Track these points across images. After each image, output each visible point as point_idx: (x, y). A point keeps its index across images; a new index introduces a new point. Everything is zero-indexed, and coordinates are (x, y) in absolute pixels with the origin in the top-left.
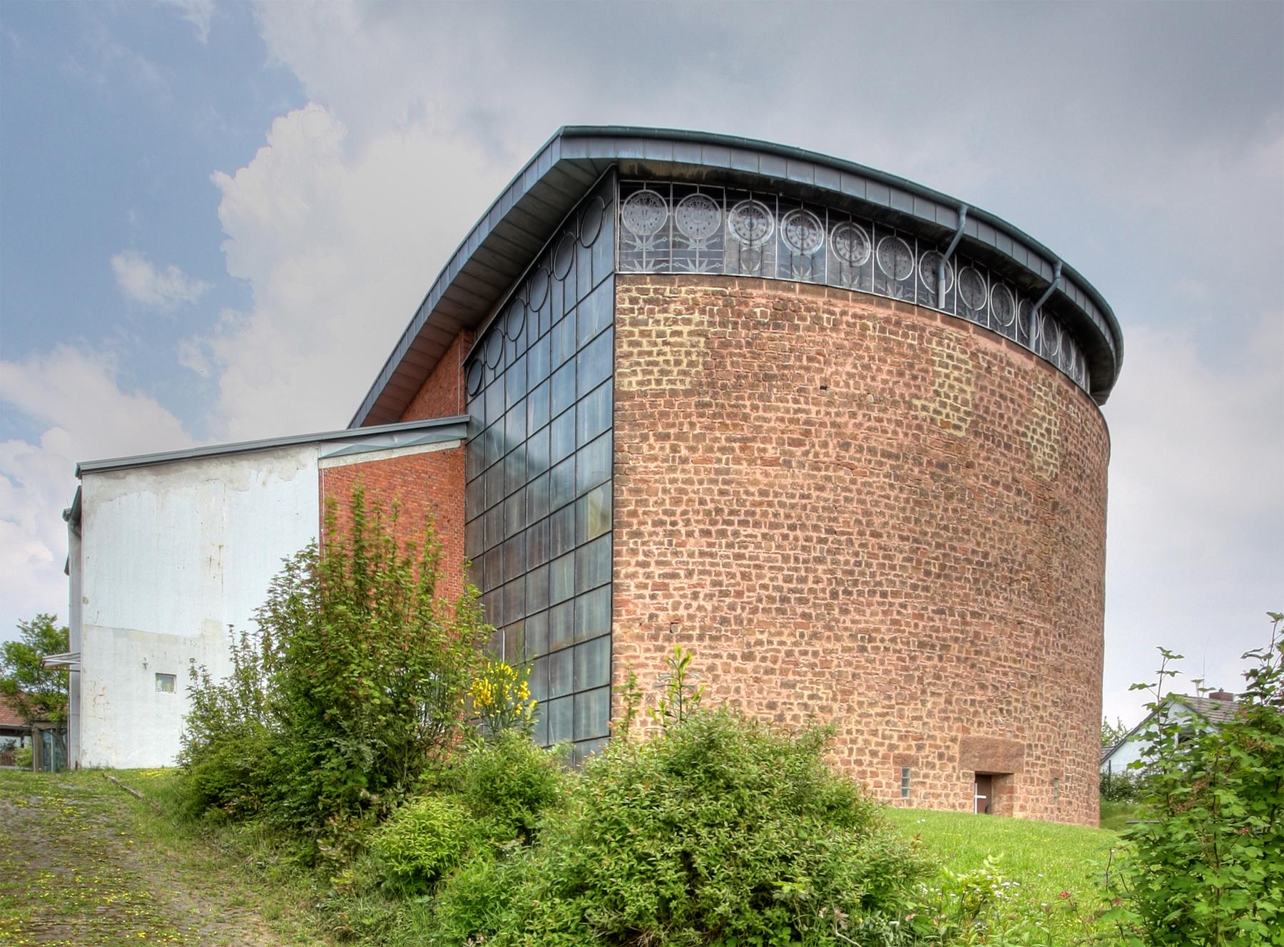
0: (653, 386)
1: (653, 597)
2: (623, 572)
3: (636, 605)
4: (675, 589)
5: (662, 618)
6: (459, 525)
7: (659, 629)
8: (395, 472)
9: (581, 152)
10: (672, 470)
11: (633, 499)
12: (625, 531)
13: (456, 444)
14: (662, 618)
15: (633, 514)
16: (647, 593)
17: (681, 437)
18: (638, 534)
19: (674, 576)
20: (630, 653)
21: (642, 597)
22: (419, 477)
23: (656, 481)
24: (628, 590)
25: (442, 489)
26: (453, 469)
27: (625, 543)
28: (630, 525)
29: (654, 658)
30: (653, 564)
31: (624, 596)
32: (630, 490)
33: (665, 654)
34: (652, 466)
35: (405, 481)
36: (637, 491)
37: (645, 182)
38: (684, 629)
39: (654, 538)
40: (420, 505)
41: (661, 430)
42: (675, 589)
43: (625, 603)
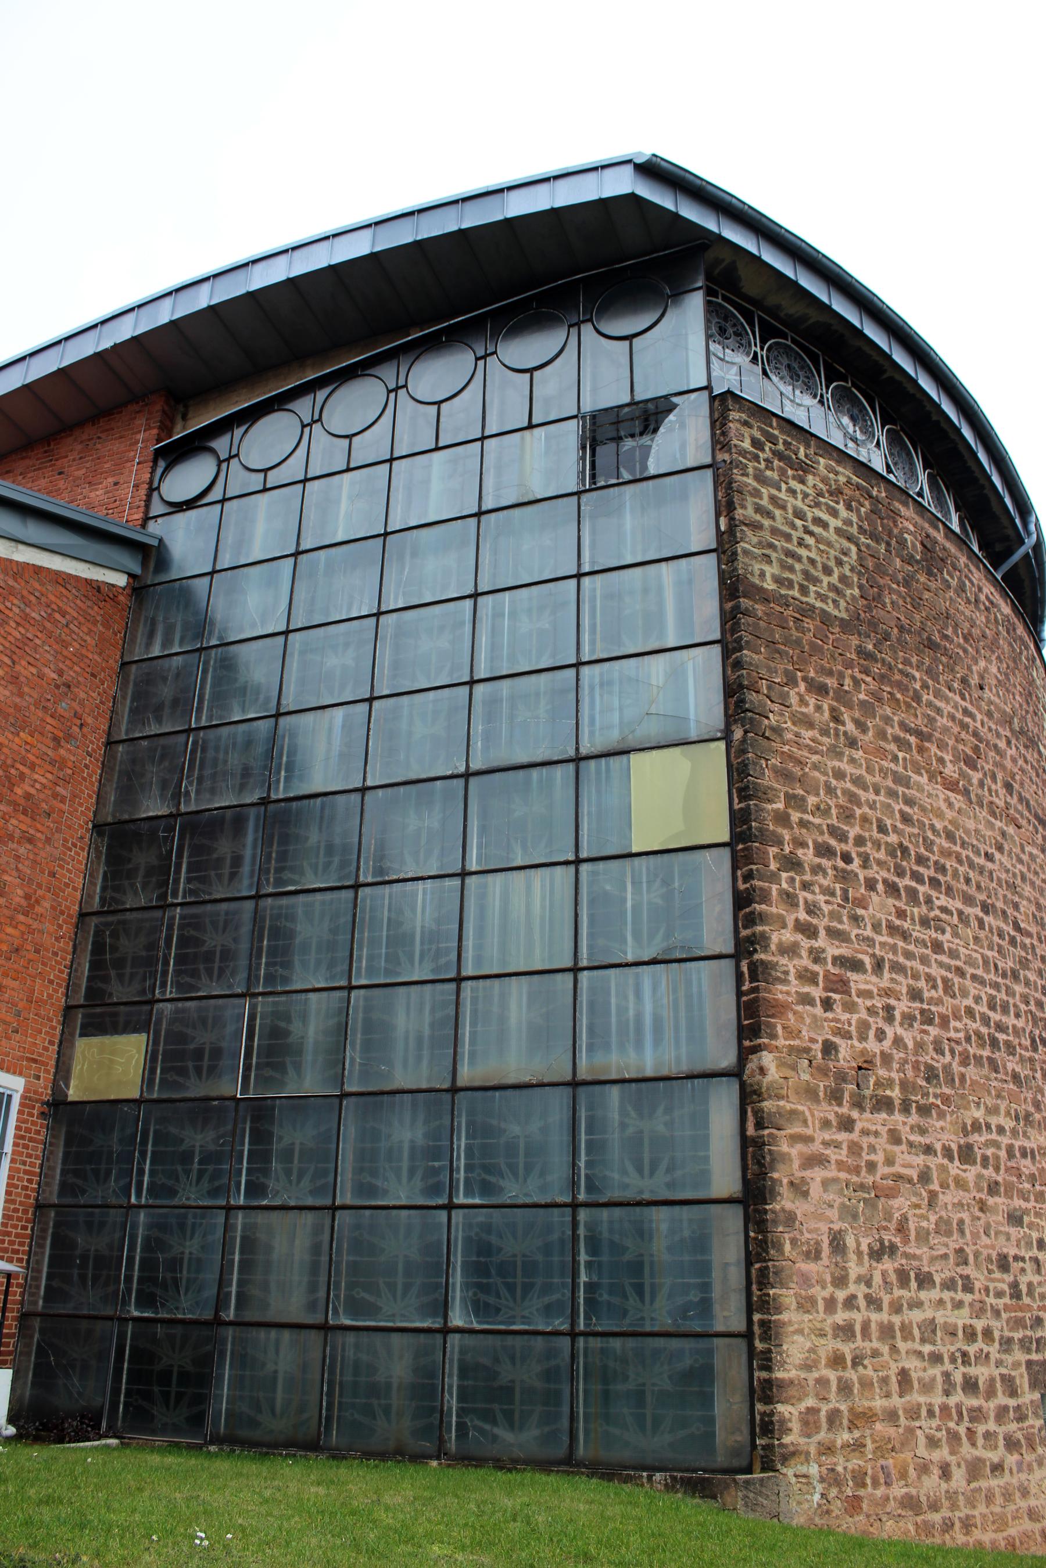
0: (796, 593)
1: (827, 1004)
2: (775, 938)
3: (800, 1017)
4: (861, 993)
5: (846, 1052)
6: (96, 742)
7: (842, 1077)
8: (11, 591)
9: (648, 191)
10: (835, 752)
11: (781, 788)
12: (773, 851)
13: (120, 580)
14: (846, 1052)
15: (782, 819)
16: (817, 992)
17: (841, 696)
18: (792, 864)
19: (857, 966)
20: (797, 1129)
21: (806, 1000)
22: (50, 618)
23: (815, 767)
24: (785, 982)
25: (83, 657)
26: (107, 625)
27: (774, 878)
28: (779, 842)
29: (838, 1145)
30: (822, 933)
31: (780, 993)
32: (776, 771)
33: (855, 1136)
34: (807, 734)
35: (26, 617)
36: (786, 776)
37: (721, 291)
38: (878, 1084)
39: (820, 878)
40: (41, 676)
41: (812, 674)
42: (861, 993)
43: (780, 1009)
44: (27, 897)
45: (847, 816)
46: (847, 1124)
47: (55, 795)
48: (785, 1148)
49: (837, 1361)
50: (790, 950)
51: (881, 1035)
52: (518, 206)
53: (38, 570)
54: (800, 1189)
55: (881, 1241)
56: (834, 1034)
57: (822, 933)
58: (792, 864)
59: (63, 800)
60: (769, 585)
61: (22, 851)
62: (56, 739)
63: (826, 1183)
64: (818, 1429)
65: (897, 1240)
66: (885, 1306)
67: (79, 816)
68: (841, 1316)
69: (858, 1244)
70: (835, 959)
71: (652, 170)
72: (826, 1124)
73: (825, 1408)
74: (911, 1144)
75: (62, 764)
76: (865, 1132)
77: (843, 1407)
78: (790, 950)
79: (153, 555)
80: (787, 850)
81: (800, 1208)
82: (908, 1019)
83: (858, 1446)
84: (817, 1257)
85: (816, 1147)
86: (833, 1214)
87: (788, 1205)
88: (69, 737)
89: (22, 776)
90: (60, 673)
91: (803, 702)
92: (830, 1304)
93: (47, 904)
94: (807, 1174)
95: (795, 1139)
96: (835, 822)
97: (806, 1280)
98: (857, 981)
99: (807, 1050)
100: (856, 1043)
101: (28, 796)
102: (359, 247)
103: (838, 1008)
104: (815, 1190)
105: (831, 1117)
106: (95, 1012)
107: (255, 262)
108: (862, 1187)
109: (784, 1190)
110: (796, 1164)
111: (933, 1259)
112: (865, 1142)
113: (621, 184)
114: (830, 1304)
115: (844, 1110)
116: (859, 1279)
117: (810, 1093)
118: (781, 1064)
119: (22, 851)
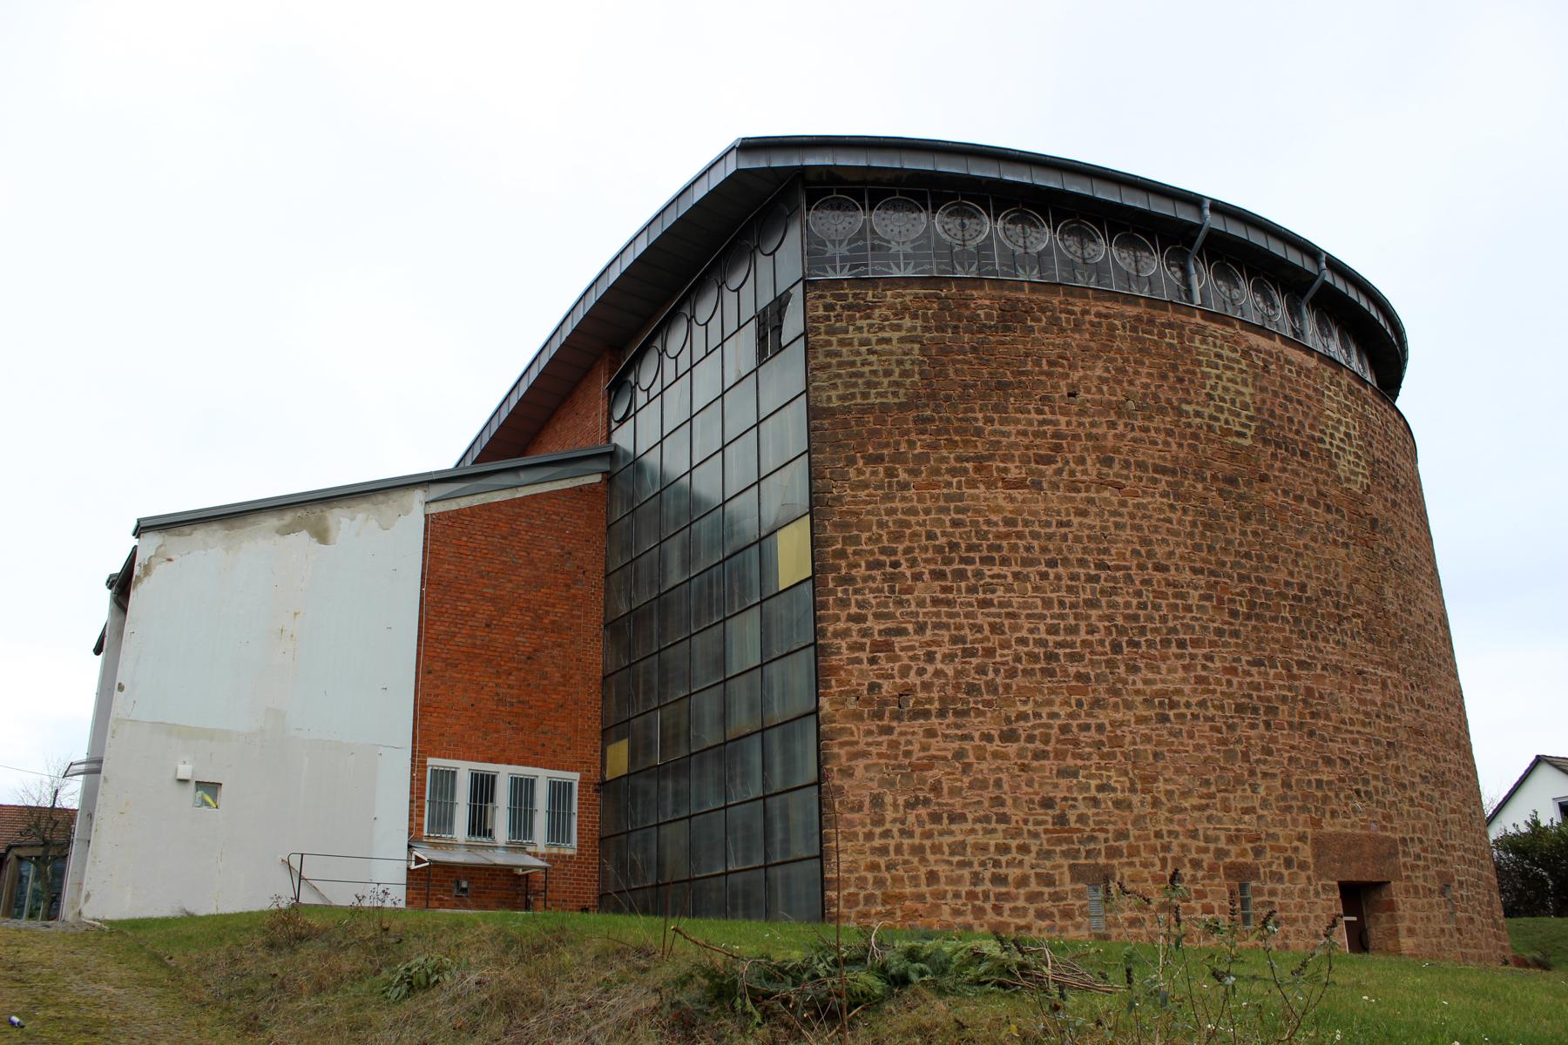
3: (850, 673)
8: (519, 515)
11: (839, 535)
13: (597, 478)
15: (841, 554)
16: (864, 656)
19: (901, 632)
23: (868, 513)
27: (833, 592)
34: (862, 494)
38: (917, 702)
44: (563, 676)
45: (897, 537)
46: (888, 730)
47: (573, 617)
48: (836, 750)
49: (874, 867)
50: (845, 633)
51: (921, 672)
52: (700, 192)
53: (535, 496)
54: (847, 773)
55: (917, 798)
56: (878, 677)
57: (870, 617)
58: (848, 580)
59: (579, 617)
60: (835, 403)
61: (555, 652)
62: (567, 586)
63: (867, 768)
64: (857, 904)
65: (931, 796)
66: (1286, 878)
67: (593, 621)
68: (877, 843)
69: (895, 800)
70: (880, 632)
71: (748, 147)
72: (869, 733)
73: (862, 894)
74: (945, 736)
75: (575, 597)
76: (902, 734)
77: (877, 892)
78: (845, 633)
79: (613, 455)
80: (843, 572)
81: (847, 783)
82: (949, 658)
83: (890, 914)
84: (860, 808)
85: (862, 747)
86: (875, 784)
87: (837, 782)
88: (576, 582)
89: (547, 613)
90: (562, 548)
91: (860, 472)
92: (869, 836)
93: (578, 677)
94: (853, 763)
95: (842, 745)
96: (886, 544)
97: (850, 823)
98: (899, 642)
99: (855, 691)
100: (897, 680)
101: (553, 622)
102: (642, 246)
103: (883, 663)
104: (859, 772)
105: (874, 728)
106: (608, 734)
107: (609, 266)
108: (900, 766)
109: (835, 774)
110: (844, 759)
111: (965, 806)
112: (902, 740)
113: (731, 166)
114: (869, 836)
115: (886, 722)
116: (894, 821)
117: (858, 717)
118: (832, 703)
119: (555, 652)
